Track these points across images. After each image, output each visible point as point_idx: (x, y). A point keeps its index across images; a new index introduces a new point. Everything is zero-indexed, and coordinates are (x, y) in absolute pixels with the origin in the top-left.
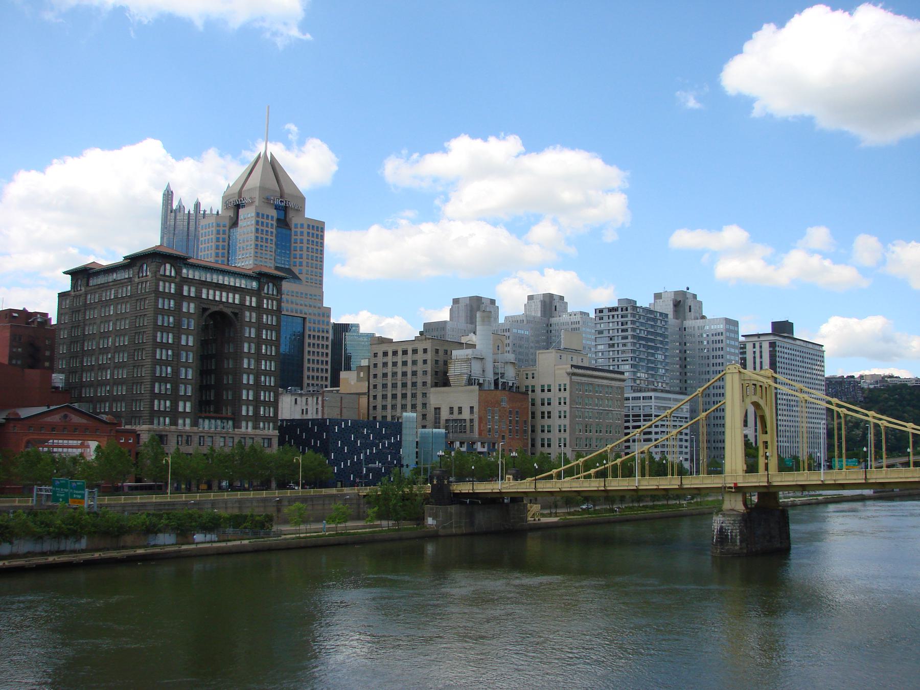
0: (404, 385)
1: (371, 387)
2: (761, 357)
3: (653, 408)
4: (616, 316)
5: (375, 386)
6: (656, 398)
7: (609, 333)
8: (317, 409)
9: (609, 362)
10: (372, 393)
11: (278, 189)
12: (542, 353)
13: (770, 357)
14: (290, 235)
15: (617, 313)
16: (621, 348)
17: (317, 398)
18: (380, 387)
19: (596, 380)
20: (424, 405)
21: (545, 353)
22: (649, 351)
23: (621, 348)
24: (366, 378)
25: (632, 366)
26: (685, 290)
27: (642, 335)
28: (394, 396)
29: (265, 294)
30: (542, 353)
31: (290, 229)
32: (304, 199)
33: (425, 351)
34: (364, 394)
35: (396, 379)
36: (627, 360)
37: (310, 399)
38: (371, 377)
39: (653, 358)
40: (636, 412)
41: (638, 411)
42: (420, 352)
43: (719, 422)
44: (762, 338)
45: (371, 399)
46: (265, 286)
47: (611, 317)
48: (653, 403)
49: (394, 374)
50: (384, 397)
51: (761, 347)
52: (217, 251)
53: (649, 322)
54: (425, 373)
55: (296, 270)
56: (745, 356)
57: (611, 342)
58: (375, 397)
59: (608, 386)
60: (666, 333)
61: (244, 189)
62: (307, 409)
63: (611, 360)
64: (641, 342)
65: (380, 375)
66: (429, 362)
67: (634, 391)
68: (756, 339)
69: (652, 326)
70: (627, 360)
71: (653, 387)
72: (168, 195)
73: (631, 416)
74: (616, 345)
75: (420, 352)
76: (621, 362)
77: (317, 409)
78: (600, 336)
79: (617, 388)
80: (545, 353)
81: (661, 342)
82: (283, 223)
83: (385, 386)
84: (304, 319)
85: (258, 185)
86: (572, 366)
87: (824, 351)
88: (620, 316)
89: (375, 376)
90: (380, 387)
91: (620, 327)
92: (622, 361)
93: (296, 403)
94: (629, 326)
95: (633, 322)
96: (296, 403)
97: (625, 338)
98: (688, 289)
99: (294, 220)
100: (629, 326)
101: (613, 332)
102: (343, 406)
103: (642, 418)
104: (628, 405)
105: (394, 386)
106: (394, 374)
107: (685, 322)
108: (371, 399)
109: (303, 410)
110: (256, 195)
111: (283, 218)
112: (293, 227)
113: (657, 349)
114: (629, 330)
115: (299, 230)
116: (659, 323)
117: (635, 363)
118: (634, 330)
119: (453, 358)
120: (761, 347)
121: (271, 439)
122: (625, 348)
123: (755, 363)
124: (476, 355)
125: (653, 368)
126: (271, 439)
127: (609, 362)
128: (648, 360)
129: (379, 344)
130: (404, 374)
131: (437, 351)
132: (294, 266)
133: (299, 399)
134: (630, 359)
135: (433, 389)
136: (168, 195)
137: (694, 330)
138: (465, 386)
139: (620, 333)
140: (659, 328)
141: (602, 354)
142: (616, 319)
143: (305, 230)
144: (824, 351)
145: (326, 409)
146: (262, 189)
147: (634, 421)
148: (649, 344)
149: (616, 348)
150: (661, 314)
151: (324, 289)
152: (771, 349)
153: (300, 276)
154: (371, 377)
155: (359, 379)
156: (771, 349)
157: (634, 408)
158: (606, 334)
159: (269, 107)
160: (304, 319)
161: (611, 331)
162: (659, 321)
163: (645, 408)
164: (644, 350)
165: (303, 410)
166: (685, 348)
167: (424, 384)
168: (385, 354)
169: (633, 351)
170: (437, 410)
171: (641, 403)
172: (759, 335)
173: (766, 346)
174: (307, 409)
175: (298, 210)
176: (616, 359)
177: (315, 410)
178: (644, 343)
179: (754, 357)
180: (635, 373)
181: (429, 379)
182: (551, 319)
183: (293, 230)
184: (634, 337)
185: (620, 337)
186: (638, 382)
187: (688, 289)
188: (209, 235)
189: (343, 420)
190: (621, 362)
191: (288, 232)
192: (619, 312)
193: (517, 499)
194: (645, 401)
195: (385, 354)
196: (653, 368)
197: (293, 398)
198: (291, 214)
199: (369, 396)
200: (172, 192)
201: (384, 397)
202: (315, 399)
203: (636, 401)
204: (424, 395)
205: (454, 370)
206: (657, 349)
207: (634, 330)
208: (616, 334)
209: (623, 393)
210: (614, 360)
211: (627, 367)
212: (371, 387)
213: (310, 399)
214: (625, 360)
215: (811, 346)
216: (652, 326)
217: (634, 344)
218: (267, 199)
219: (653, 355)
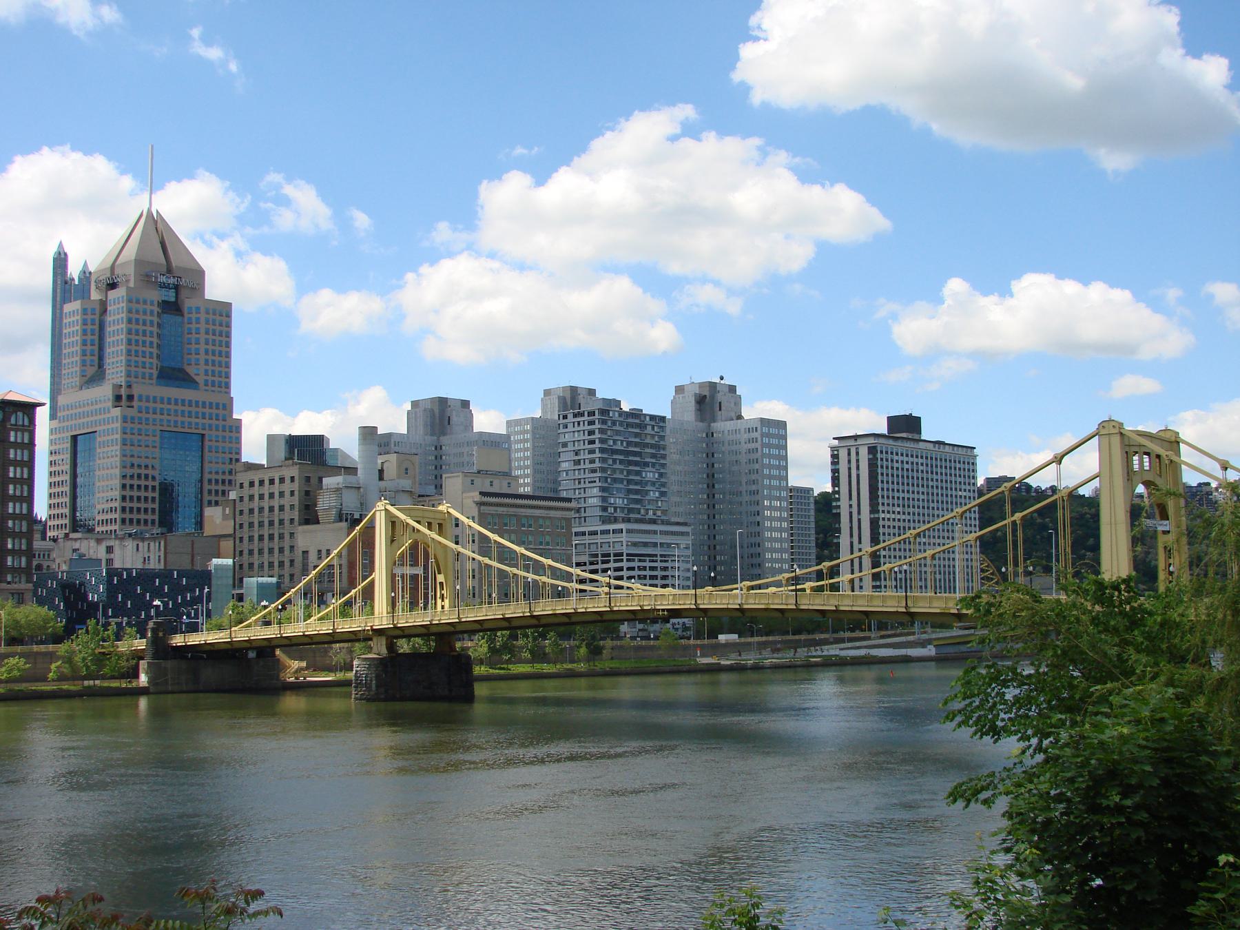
0: (271, 523)
1: (237, 527)
2: (858, 468)
3: (624, 544)
4: (582, 423)
5: (241, 526)
6: (629, 531)
7: (574, 445)
8: (159, 556)
9: (574, 484)
10: (238, 535)
11: (163, 261)
12: (449, 477)
13: (869, 468)
14: (183, 323)
15: (582, 419)
16: (588, 466)
17: (160, 543)
18: (246, 526)
19: (522, 510)
20: (292, 547)
21: (454, 477)
22: (630, 468)
23: (588, 466)
24: (232, 515)
25: (603, 489)
26: (717, 380)
27: (618, 447)
28: (261, 538)
29: (12, 425)
30: (449, 477)
31: (182, 315)
32: (204, 271)
33: (292, 479)
34: (229, 536)
35: (263, 517)
36: (595, 482)
37: (152, 544)
38: (237, 513)
39: (638, 478)
40: (605, 549)
41: (607, 548)
42: (288, 480)
43: (755, 561)
44: (859, 442)
45: (237, 541)
46: (11, 415)
47: (576, 424)
48: (624, 537)
49: (261, 509)
50: (251, 538)
51: (857, 453)
52: (85, 348)
53: (630, 430)
54: (292, 507)
55: (191, 371)
56: (837, 467)
57: (577, 458)
58: (241, 539)
59: (543, 518)
60: (662, 443)
61: (118, 262)
62: (149, 557)
63: (577, 482)
64: (615, 457)
65: (246, 511)
66: (296, 493)
67: (604, 522)
68: (852, 442)
69: (636, 435)
70: (595, 482)
71: (639, 516)
72: (61, 261)
73: (600, 555)
74: (582, 461)
75: (288, 480)
76: (587, 485)
77: (159, 556)
78: (564, 449)
79: (561, 519)
80: (454, 477)
81: (653, 456)
82: (172, 308)
83: (251, 525)
84: (203, 435)
85: (133, 258)
86: (482, 494)
87: (976, 456)
88: (586, 423)
89: (241, 512)
90: (246, 526)
91: (587, 437)
92: (589, 482)
93: (138, 549)
94: (597, 435)
95: (602, 431)
96: (138, 549)
97: (592, 452)
98: (722, 378)
99: (188, 303)
100: (597, 435)
101: (578, 445)
102: (195, 552)
103: (612, 558)
104: (596, 541)
105: (261, 524)
106: (261, 509)
107: (712, 424)
108: (237, 541)
109: (145, 558)
110: (131, 271)
111: (173, 299)
112: (186, 311)
113: (646, 464)
114: (597, 441)
115: (194, 316)
116: (649, 430)
117: (606, 485)
118: (602, 441)
119: (324, 487)
120: (857, 453)
121: (23, 594)
122: (592, 465)
123: (850, 476)
124: (350, 483)
125: (637, 492)
126: (23, 594)
127: (574, 484)
128: (629, 482)
129: (246, 471)
130: (271, 509)
131: (308, 479)
132: (188, 364)
133: (141, 544)
134: (597, 480)
135: (300, 528)
136: (61, 261)
137: (723, 434)
138: (333, 522)
139: (587, 446)
140: (649, 437)
141: (567, 475)
142: (581, 427)
143: (203, 316)
144: (976, 456)
145: (169, 556)
146: (139, 262)
147: (615, 561)
148: (631, 458)
149: (582, 466)
150: (652, 417)
151: (234, 392)
152: (871, 456)
153: (196, 378)
154: (237, 513)
155: (225, 517)
156: (871, 456)
157: (603, 545)
158: (570, 447)
159: (152, 146)
160: (203, 435)
161: (576, 443)
162: (649, 428)
163: (616, 544)
164: (622, 467)
165: (145, 558)
166: (713, 460)
167: (292, 521)
168: (262, 483)
169: (603, 470)
170: (305, 553)
171: (611, 538)
172: (856, 437)
173: (864, 452)
174: (149, 557)
175: (193, 289)
176: (582, 481)
177: (157, 558)
178: (621, 457)
179: (850, 469)
180: (604, 499)
181: (296, 515)
182: (441, 438)
183: (186, 315)
184: (602, 450)
185: (586, 451)
186: (611, 510)
187: (722, 378)
188: (118, 314)
189: (126, 570)
190: (587, 485)
191: (179, 319)
192: (586, 418)
193: (266, 649)
194: (615, 535)
195: (252, 484)
196: (637, 492)
197: (135, 543)
198: (184, 293)
199: (235, 538)
200: (66, 254)
201: (251, 538)
202: (157, 544)
203: (593, 537)
204: (292, 534)
205: (325, 503)
206: (646, 464)
207: (602, 441)
208: (582, 447)
209: (569, 527)
210: (579, 483)
211: (595, 491)
212: (237, 527)
213: (152, 544)
214: (592, 482)
215: (960, 451)
216: (636, 435)
217: (603, 460)
218: (147, 276)
219: (638, 473)
